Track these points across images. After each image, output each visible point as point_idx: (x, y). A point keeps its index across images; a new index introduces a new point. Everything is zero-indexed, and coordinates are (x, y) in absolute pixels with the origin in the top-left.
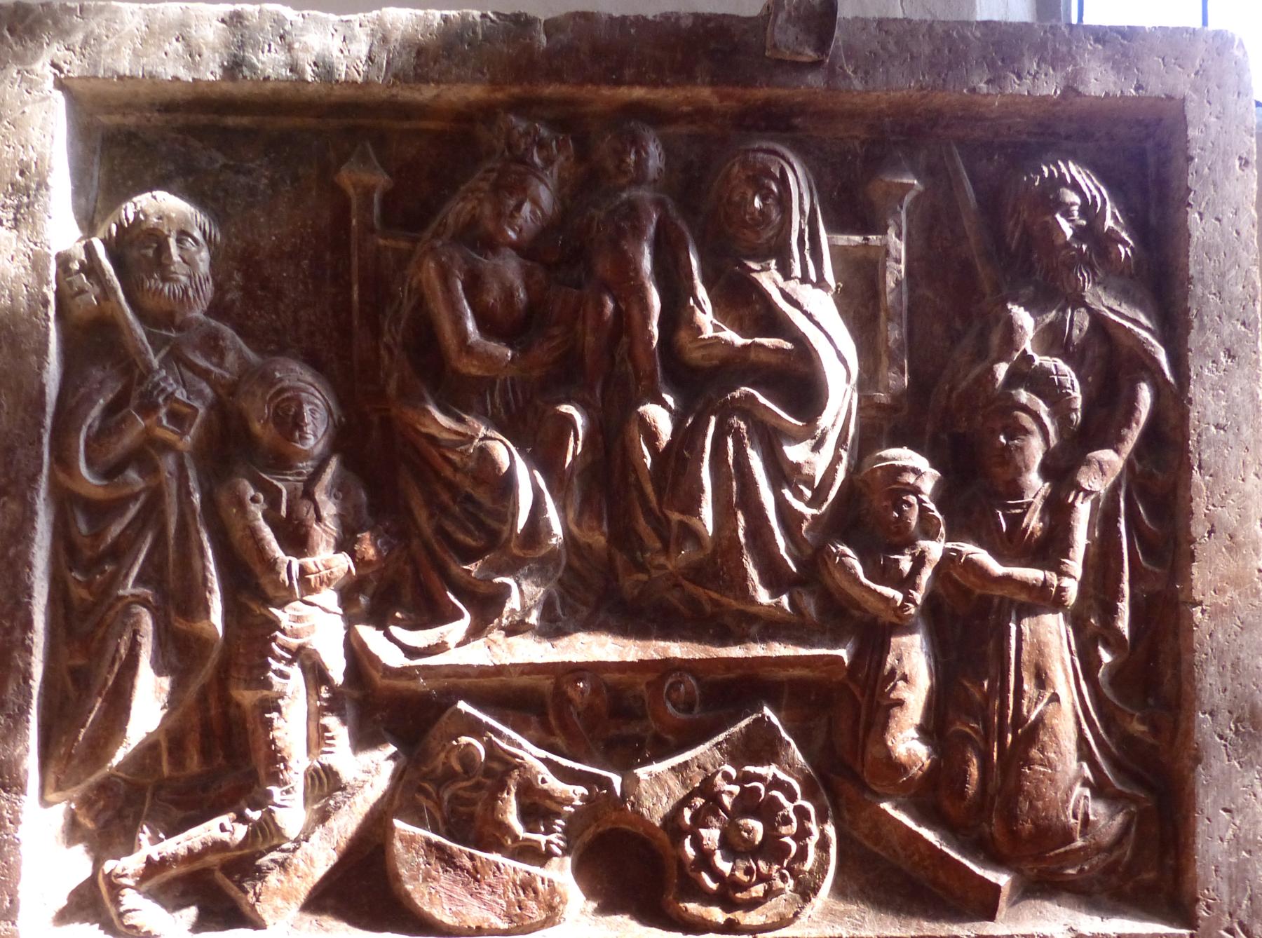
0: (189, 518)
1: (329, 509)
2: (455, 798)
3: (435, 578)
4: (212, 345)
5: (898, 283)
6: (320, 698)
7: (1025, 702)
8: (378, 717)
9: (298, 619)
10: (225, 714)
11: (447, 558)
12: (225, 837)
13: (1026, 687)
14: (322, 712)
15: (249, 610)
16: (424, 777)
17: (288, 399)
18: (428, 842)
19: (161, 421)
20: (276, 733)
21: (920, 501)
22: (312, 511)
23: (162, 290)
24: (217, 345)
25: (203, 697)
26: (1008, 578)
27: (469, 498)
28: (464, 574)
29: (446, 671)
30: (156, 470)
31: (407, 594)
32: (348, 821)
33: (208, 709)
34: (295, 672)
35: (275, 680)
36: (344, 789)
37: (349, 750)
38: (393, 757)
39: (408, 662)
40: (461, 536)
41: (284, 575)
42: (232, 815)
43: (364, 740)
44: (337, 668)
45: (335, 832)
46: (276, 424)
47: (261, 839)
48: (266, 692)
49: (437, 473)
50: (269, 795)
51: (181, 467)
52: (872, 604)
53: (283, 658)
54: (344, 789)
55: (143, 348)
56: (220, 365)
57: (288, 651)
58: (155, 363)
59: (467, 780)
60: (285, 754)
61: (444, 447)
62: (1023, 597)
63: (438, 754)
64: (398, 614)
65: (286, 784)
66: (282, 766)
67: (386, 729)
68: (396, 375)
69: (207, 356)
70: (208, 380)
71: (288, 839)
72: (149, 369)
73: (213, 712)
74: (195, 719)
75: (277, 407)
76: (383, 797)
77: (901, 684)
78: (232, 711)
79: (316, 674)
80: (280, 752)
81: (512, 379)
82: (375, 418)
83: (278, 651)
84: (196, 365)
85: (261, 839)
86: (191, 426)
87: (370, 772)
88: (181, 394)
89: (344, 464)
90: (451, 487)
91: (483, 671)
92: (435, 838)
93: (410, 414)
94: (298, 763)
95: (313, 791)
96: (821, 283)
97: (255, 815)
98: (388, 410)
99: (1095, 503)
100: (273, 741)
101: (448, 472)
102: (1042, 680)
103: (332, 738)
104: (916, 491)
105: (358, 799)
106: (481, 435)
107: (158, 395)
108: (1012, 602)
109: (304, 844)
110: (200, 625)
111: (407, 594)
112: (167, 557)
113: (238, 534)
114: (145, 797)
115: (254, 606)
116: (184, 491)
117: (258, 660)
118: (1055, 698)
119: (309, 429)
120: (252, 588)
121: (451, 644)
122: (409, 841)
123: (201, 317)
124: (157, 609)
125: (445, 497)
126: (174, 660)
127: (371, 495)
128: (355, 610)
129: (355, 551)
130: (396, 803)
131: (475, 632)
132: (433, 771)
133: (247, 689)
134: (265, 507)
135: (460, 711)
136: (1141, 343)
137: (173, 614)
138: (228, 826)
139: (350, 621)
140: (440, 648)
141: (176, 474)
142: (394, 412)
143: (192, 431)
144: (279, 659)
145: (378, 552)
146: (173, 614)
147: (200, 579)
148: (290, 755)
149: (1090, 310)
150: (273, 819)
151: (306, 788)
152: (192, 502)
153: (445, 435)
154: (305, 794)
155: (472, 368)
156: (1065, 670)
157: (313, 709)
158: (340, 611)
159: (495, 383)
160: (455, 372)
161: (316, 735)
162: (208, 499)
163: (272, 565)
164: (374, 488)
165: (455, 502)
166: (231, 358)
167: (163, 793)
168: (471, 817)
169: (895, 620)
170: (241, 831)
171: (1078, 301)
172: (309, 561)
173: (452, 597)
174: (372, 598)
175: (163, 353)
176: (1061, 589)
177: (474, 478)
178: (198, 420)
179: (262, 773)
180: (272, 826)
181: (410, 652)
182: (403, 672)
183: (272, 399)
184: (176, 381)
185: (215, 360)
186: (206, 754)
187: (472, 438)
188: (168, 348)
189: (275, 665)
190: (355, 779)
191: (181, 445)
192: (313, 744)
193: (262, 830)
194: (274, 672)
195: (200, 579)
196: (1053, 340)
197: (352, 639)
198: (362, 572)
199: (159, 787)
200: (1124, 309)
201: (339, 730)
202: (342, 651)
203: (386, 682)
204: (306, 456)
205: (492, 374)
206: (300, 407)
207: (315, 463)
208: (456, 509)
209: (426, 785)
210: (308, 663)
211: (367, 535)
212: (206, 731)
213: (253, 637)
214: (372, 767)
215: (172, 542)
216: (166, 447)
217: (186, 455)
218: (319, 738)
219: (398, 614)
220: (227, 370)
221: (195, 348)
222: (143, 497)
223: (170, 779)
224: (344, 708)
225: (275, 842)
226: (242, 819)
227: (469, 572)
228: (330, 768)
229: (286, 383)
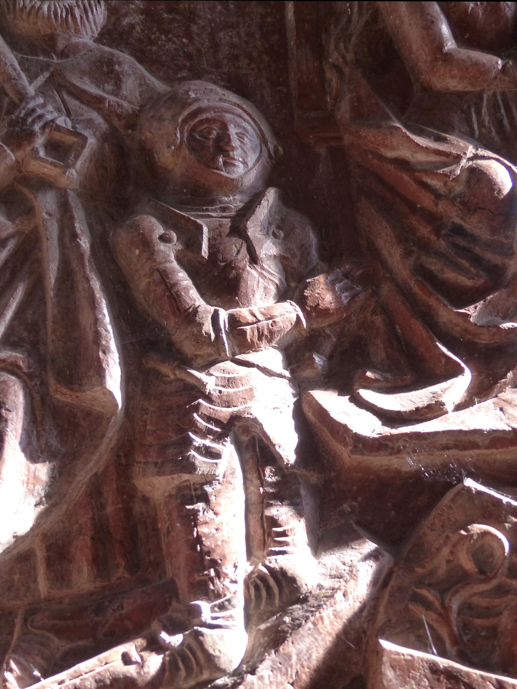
0: (74, 264)
1: (268, 249)
2: (467, 607)
3: (418, 327)
4: (106, 71)
6: (263, 483)
8: (346, 507)
9: (230, 382)
10: (127, 510)
11: (432, 302)
12: (132, 670)
14: (266, 501)
15: (158, 375)
16: (420, 582)
17: (207, 120)
18: (434, 669)
19: (37, 152)
20: (203, 530)
22: (244, 251)
23: (40, 8)
24: (112, 71)
25: (95, 490)
27: (458, 230)
28: (460, 320)
29: (444, 441)
30: (30, 211)
31: (378, 350)
32: (311, 645)
33: (103, 507)
34: (228, 450)
35: (199, 460)
36: (304, 600)
37: (308, 550)
38: (373, 556)
39: (387, 431)
40: (450, 275)
41: (208, 327)
42: (140, 642)
43: (323, 540)
44: (286, 442)
45: (294, 658)
46: (192, 150)
47: (183, 673)
48: (185, 477)
49: (412, 206)
50: (197, 612)
51: (64, 207)
53: (209, 431)
54: (304, 600)
55: (14, 74)
56: (116, 93)
57: (217, 422)
58: (31, 90)
59: (484, 581)
60: (216, 557)
61: (419, 171)
63: (439, 550)
64: (369, 374)
65: (218, 596)
66: (212, 573)
67: (358, 523)
68: (348, 96)
69: (98, 83)
70: (99, 110)
71: (223, 672)
72: (23, 97)
73: (109, 509)
74: (85, 519)
75: (193, 129)
76: (362, 609)
78: (137, 508)
79: (257, 450)
80: (208, 553)
81: (503, 94)
82: (323, 151)
83: (202, 423)
84: (84, 92)
85: (183, 673)
86: (77, 157)
87: (341, 578)
88: (62, 121)
89: (286, 199)
90: (432, 219)
91: (497, 439)
92: (443, 662)
93: (370, 135)
94: (237, 565)
95: (257, 606)
97: (175, 640)
98: (340, 139)
100: (199, 540)
101: (426, 201)
103: (284, 534)
105: (327, 613)
106: (469, 155)
107: (33, 122)
109: (249, 678)
110: (89, 395)
111: (378, 350)
112: (44, 315)
113: (141, 284)
114: (13, 625)
115: (165, 369)
116: (67, 232)
117: (174, 438)
119: (237, 154)
120: (162, 347)
121: (449, 406)
122: (406, 668)
123: (91, 43)
124: (30, 376)
125: (424, 231)
126: (54, 442)
127: (321, 238)
128: (307, 373)
129: (306, 298)
130: (381, 618)
131: (479, 392)
132: (432, 573)
133: (160, 473)
134: (180, 247)
135: (469, 489)
137: (52, 381)
138: (135, 656)
139: (301, 386)
140: (434, 410)
141: (57, 215)
142: (347, 139)
143: (79, 163)
144: (204, 433)
145: (337, 298)
146: (52, 381)
147: (90, 336)
148: (224, 557)
150: (201, 645)
151: (248, 601)
152: (79, 246)
153: (421, 157)
154: (246, 609)
155: (452, 83)
157: (254, 498)
158: (287, 374)
159: (481, 98)
160: (427, 89)
161: (260, 531)
162: (103, 246)
163: (191, 316)
164: (322, 227)
165: (439, 236)
166: (129, 85)
167: (38, 618)
168: (493, 632)
170: (154, 662)
172: (243, 312)
173: (444, 349)
174: (327, 356)
175: (40, 80)
177: (464, 204)
178: (86, 152)
179: (182, 584)
180: (199, 654)
181: (389, 418)
182: (380, 445)
183: (185, 121)
184: (59, 110)
185: (109, 87)
186: (100, 563)
187: (458, 158)
188: (47, 75)
189: (198, 441)
190: (320, 587)
191: (63, 181)
192: (255, 544)
193: (185, 659)
194: (198, 449)
195: (90, 336)
197: (306, 409)
198: (315, 326)
199: (32, 612)
201: (295, 526)
202: (292, 423)
203: (358, 458)
204: (232, 186)
205: (478, 89)
206: (224, 127)
207: (246, 199)
208: (442, 244)
209: (424, 592)
210: (245, 439)
211: (321, 278)
212: (101, 534)
213: (169, 408)
214: (344, 570)
215: (51, 293)
216: (43, 184)
217: (71, 193)
218: (264, 535)
219: (369, 374)
220: (125, 98)
221: (83, 73)
222: (11, 245)
223: (49, 600)
224: (299, 495)
225: (205, 676)
226: (154, 645)
227: (467, 316)
228: (283, 572)
229: (204, 103)
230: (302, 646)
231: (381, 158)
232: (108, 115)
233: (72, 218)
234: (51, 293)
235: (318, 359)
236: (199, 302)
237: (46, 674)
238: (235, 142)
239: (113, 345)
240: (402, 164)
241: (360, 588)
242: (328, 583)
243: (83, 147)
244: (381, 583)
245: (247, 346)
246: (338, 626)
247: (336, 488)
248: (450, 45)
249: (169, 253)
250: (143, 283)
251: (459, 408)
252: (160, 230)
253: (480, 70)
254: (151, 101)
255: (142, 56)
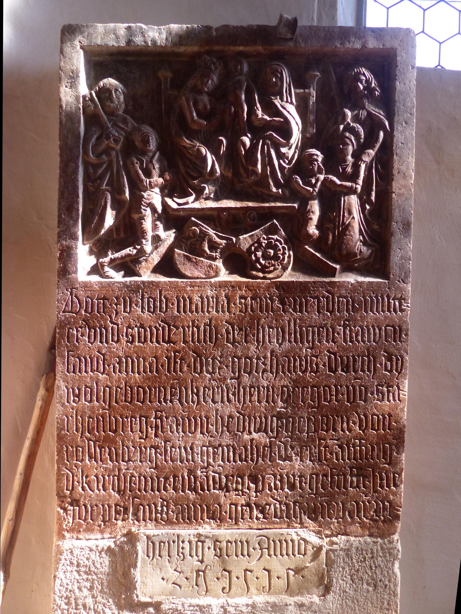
1: (157, 166)
4: (125, 121)
5: (313, 103)
6: (155, 217)
7: (345, 219)
8: (170, 222)
9: (149, 195)
12: (131, 253)
13: (345, 215)
15: (136, 193)
18: (184, 255)
20: (144, 226)
21: (318, 164)
25: (124, 217)
26: (342, 185)
27: (195, 163)
30: (110, 155)
32: (163, 249)
35: (143, 211)
36: (162, 241)
37: (163, 231)
38: (174, 232)
40: (192, 173)
41: (145, 183)
42: (132, 247)
44: (159, 209)
50: (142, 242)
51: (117, 154)
52: (304, 192)
54: (162, 241)
56: (127, 127)
58: (110, 126)
62: (345, 190)
77: (311, 214)
79: (154, 210)
87: (168, 236)
88: (116, 134)
89: (161, 154)
90: (190, 160)
91: (198, 210)
92: (186, 254)
94: (150, 234)
96: (291, 103)
97: (139, 247)
99: (366, 165)
100: (143, 228)
101: (189, 156)
102: (350, 213)
104: (317, 161)
105: (166, 243)
108: (342, 192)
110: (123, 197)
113: (133, 173)
115: (137, 192)
118: (353, 218)
119: (151, 144)
120: (137, 188)
121: (190, 202)
122: (179, 254)
123: (122, 113)
125: (188, 163)
128: (164, 194)
131: (196, 199)
136: (381, 120)
138: (132, 250)
139: (163, 196)
140: (187, 203)
145: (170, 177)
149: (367, 110)
150: (143, 248)
153: (188, 146)
155: (195, 127)
156: (356, 211)
163: (142, 181)
166: (130, 125)
168: (196, 248)
169: (310, 196)
170: (135, 251)
171: (364, 108)
172: (152, 180)
174: (169, 190)
175: (111, 123)
176: (356, 188)
178: (121, 141)
179: (140, 236)
181: (179, 204)
185: (126, 125)
186: (125, 232)
187: (195, 146)
189: (143, 208)
196: (356, 119)
200: (377, 110)
201: (161, 226)
202: (161, 204)
204: (150, 151)
210: (152, 207)
211: (167, 173)
213: (137, 199)
214: (169, 235)
215: (115, 175)
216: (113, 149)
218: (155, 227)
222: (107, 163)
226: (135, 248)
229: (145, 131)
230: (161, 249)
231: (181, 145)
232: (126, 132)
233: (119, 157)
234: (115, 175)
235: (166, 191)
236: (144, 178)
237: (116, 253)
238: (151, 141)
239: (127, 186)
240: (184, 147)
241: (172, 239)
242: (166, 237)
243: (120, 140)
244: (176, 238)
245: (153, 188)
246: (168, 246)
247: (169, 218)
248: (196, 118)
249: (138, 166)
250: (133, 173)
251: (192, 203)
252: (136, 161)
253: (200, 124)
254: (134, 128)
255: (132, 117)
